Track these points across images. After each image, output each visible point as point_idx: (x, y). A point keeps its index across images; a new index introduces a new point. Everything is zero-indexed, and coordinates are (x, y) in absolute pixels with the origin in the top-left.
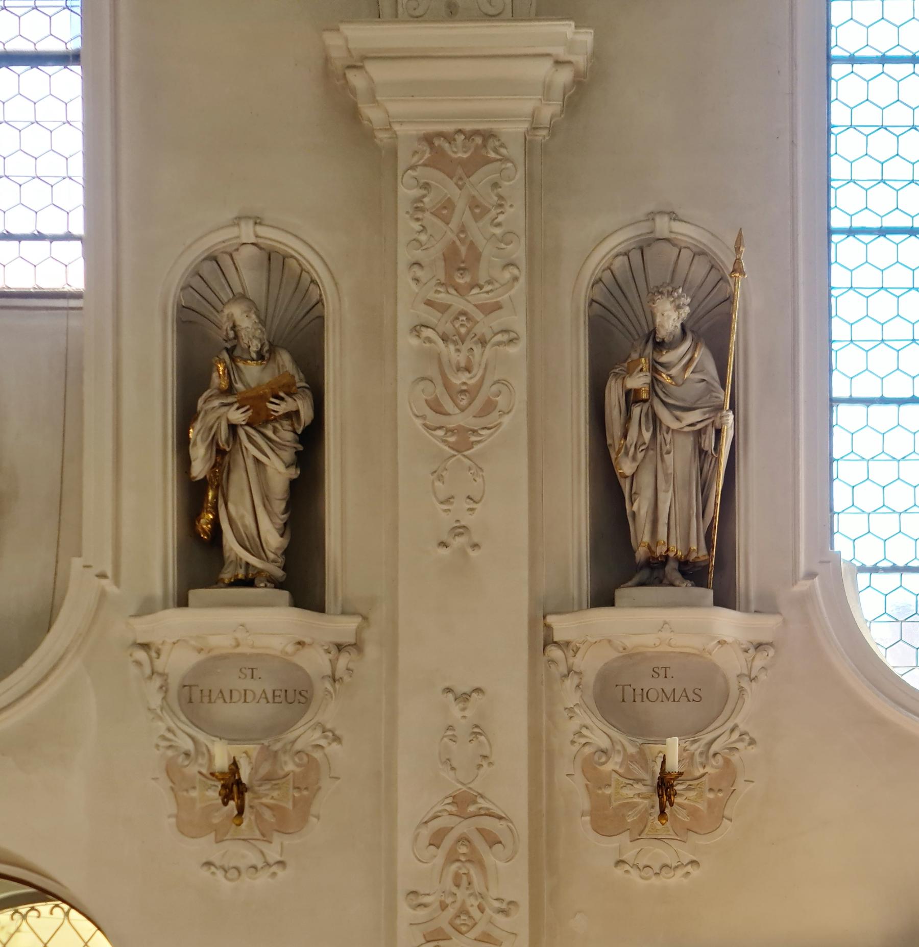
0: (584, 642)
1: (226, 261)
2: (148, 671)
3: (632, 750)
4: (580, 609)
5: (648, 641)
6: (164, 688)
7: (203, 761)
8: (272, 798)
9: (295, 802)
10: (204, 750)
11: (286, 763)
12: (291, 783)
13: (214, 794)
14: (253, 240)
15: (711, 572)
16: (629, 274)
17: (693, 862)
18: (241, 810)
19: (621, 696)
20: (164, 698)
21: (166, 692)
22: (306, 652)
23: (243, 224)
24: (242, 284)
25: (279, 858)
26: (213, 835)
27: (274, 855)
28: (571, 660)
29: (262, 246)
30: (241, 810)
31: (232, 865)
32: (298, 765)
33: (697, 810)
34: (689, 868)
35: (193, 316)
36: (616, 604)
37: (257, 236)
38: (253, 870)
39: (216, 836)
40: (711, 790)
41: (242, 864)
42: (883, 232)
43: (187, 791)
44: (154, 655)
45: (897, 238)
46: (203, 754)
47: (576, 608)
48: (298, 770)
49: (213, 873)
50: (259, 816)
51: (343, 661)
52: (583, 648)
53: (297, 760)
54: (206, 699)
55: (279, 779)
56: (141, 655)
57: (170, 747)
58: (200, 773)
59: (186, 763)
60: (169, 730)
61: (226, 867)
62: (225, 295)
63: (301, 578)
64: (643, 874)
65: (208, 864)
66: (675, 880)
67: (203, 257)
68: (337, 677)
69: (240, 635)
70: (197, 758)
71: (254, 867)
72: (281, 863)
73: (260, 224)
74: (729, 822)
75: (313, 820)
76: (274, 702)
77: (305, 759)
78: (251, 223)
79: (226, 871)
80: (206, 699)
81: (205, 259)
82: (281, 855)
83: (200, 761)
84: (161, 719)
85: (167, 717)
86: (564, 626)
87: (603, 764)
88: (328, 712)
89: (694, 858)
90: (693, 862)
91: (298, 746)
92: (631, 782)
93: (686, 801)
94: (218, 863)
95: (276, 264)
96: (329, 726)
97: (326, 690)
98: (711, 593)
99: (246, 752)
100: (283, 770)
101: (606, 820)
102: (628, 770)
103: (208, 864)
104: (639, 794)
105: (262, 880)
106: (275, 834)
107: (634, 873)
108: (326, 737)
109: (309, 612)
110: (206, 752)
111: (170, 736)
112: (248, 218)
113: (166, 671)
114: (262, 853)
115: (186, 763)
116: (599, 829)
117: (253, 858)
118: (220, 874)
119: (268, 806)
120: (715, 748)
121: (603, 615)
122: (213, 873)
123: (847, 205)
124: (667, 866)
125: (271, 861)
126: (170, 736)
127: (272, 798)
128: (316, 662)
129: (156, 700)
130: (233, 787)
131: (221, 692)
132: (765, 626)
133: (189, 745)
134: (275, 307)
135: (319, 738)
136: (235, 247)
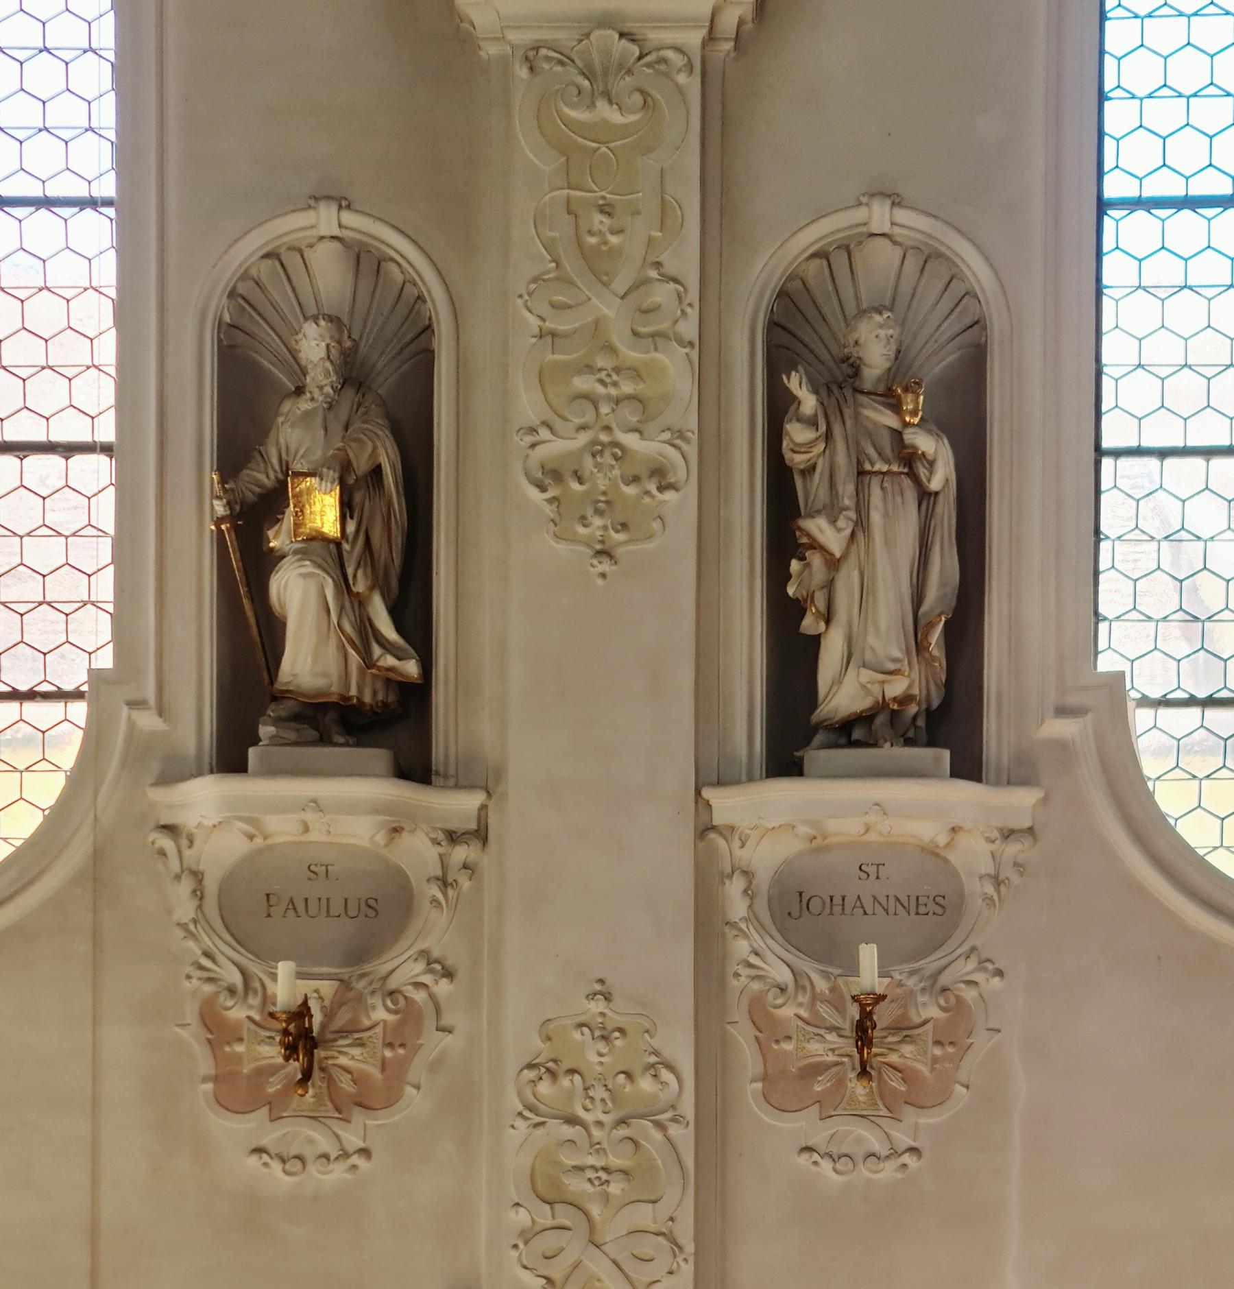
0: (755, 828)
1: (293, 261)
2: (175, 866)
3: (822, 985)
4: (751, 779)
5: (846, 827)
6: (199, 894)
7: (255, 1001)
8: (902, 1056)
9: (384, 1065)
10: (257, 985)
11: (374, 1007)
12: (930, 1035)
13: (272, 1053)
14: (336, 232)
15: (948, 724)
16: (893, 276)
17: (913, 1150)
18: (307, 1075)
19: (807, 910)
20: (200, 907)
21: (201, 898)
22: (406, 839)
23: (322, 206)
24: (856, 295)
25: (361, 1144)
26: (265, 1110)
27: (353, 1140)
28: (187, 853)
29: (898, 239)
30: (307, 1075)
31: (293, 1152)
32: (944, 1010)
33: (917, 1073)
34: (355, 1160)
35: (240, 338)
36: (806, 768)
37: (340, 226)
38: (324, 1160)
39: (270, 1110)
40: (938, 1043)
41: (308, 1152)
42: (46, 203)
43: (777, 1041)
44: (184, 842)
45: (65, 212)
46: (256, 992)
47: (744, 778)
48: (390, 1018)
49: (266, 1164)
50: (331, 1082)
51: (460, 853)
52: (754, 835)
53: (389, 1003)
54: (837, 909)
55: (363, 1031)
56: (166, 843)
57: (758, 977)
58: (249, 1018)
59: (229, 1003)
60: (207, 955)
61: (285, 1155)
62: (289, 308)
63: (392, 724)
64: (838, 1166)
65: (809, 1149)
66: (888, 1171)
67: (261, 253)
68: (450, 880)
69: (872, 818)
70: (796, 996)
71: (325, 1156)
72: (365, 1152)
73: (348, 207)
74: (414, 1091)
75: (410, 1091)
76: (917, 914)
77: (402, 1002)
78: (888, 203)
79: (284, 1161)
80: (837, 909)
81: (814, 255)
82: (364, 1141)
83: (801, 999)
84: (746, 936)
85: (757, 937)
86: (728, 804)
87: (780, 1006)
88: (435, 930)
89: (914, 1144)
90: (913, 1150)
91: (393, 984)
92: (822, 1032)
93: (901, 1060)
94: (273, 1151)
95: (367, 266)
96: (436, 954)
97: (434, 900)
98: (946, 754)
99: (317, 991)
100: (369, 1017)
101: (789, 1086)
102: (815, 1013)
103: (259, 1150)
104: (833, 1050)
105: (337, 1173)
106: (357, 1110)
107: (826, 1165)
108: (432, 971)
109: (415, 785)
110: (807, 984)
111: (205, 962)
112: (329, 198)
113: (201, 868)
114: (337, 1136)
115: (780, 1001)
116: (223, 1103)
117: (325, 1144)
118: (276, 1166)
119: (347, 1070)
120: (944, 980)
121: (785, 790)
122: (266, 1164)
123: (1129, 165)
124: (874, 1155)
125: (351, 1150)
126: (205, 962)
127: (353, 1058)
128: (418, 854)
129: (185, 910)
130: (301, 1037)
131: (292, 901)
132: (1020, 802)
133: (785, 976)
134: (364, 327)
135: (425, 972)
136: (308, 241)
